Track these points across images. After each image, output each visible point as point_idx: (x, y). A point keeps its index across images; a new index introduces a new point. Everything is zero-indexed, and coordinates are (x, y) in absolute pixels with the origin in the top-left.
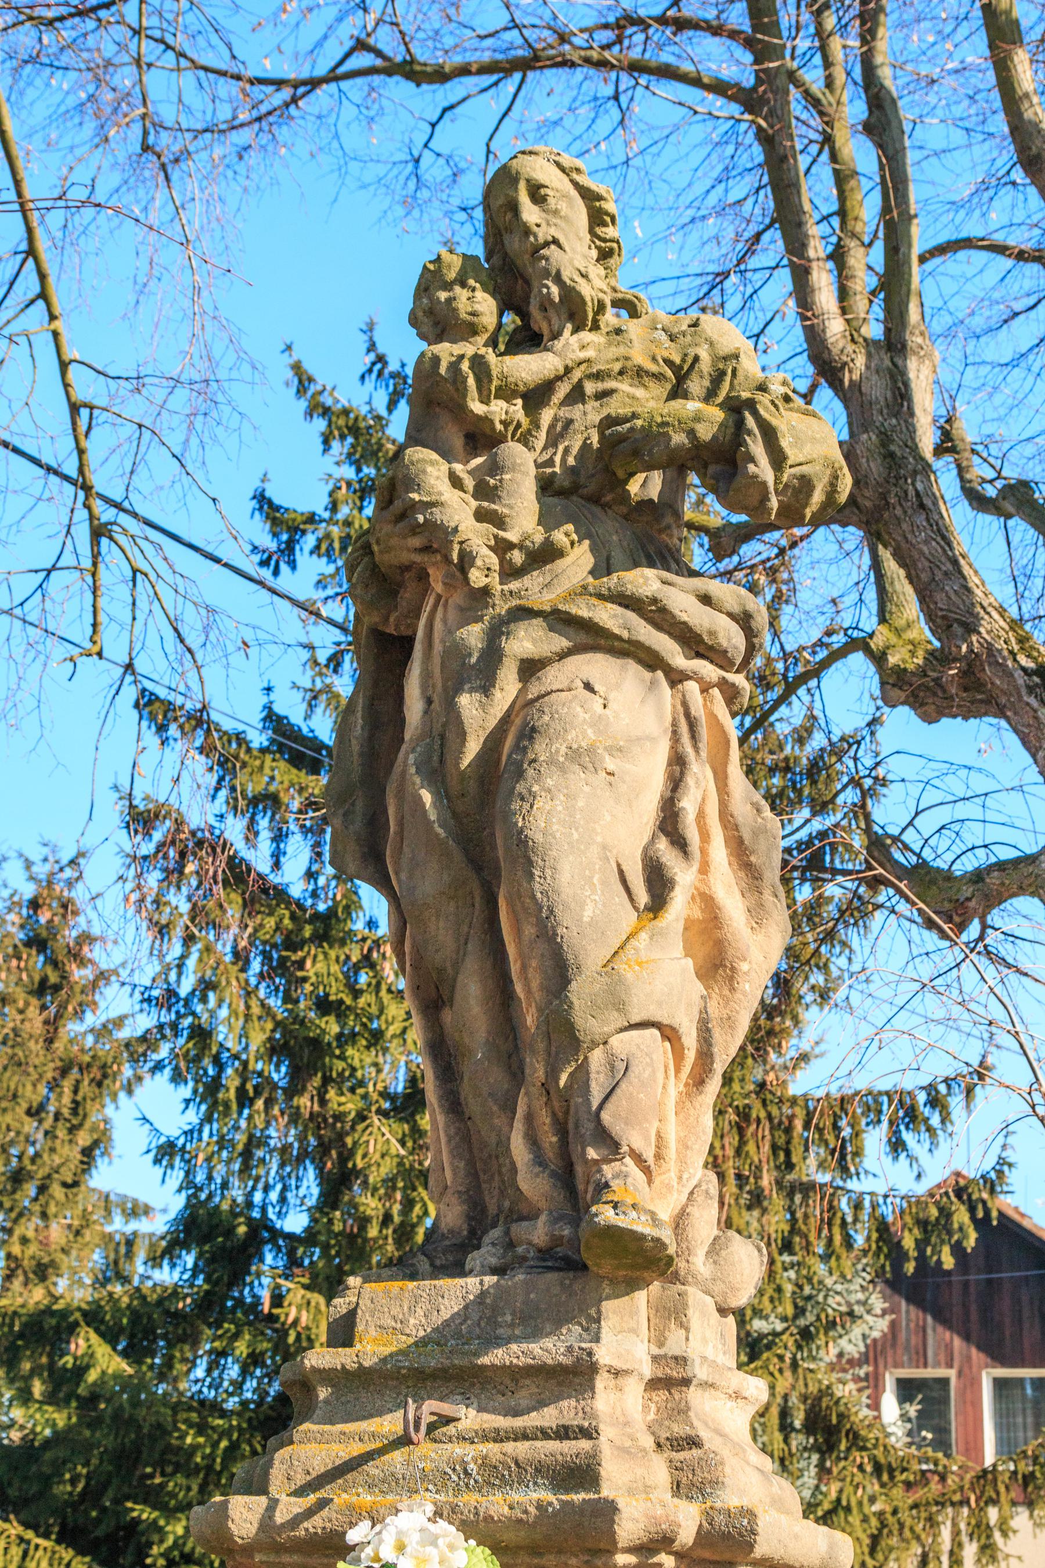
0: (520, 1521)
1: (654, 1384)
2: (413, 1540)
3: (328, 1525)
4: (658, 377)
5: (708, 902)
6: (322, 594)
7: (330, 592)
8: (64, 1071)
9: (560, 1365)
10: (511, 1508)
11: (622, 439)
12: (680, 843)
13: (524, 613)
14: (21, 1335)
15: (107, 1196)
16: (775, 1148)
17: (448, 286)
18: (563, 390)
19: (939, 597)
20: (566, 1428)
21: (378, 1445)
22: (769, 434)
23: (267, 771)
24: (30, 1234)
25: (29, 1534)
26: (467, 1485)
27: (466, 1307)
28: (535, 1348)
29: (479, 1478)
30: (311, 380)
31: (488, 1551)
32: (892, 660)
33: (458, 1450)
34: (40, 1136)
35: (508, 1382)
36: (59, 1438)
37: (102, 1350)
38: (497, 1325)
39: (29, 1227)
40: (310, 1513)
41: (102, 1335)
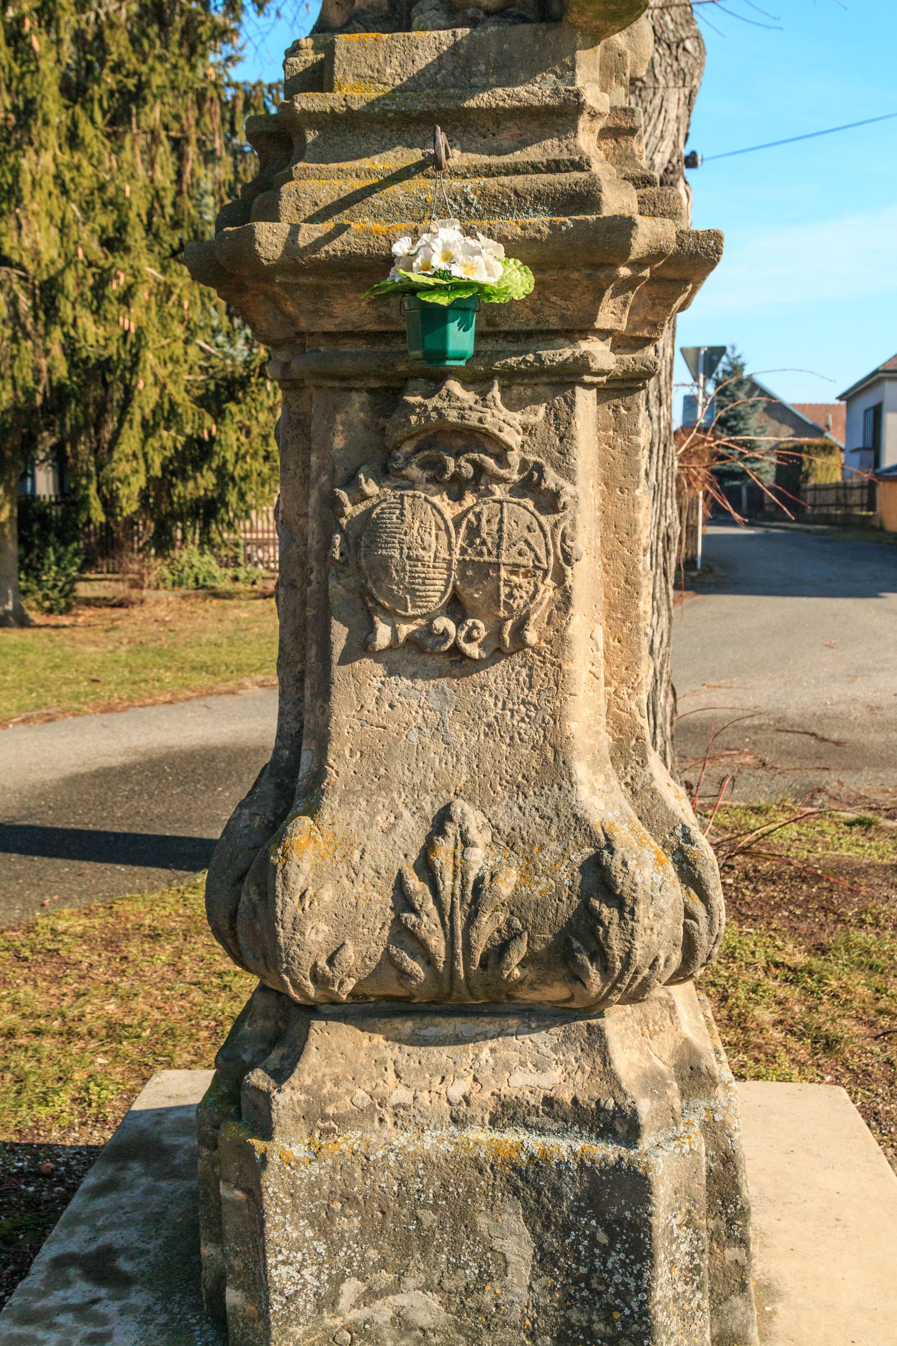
0: (534, 240)
2: (456, 252)
3: (347, 248)
9: (547, 106)
10: (523, 228)
16: (223, 119)
20: (557, 162)
21: (375, 181)
26: (468, 213)
27: (440, 58)
28: (521, 90)
29: (480, 207)
31: (519, 263)
35: (490, 125)
38: (472, 75)
40: (330, 237)
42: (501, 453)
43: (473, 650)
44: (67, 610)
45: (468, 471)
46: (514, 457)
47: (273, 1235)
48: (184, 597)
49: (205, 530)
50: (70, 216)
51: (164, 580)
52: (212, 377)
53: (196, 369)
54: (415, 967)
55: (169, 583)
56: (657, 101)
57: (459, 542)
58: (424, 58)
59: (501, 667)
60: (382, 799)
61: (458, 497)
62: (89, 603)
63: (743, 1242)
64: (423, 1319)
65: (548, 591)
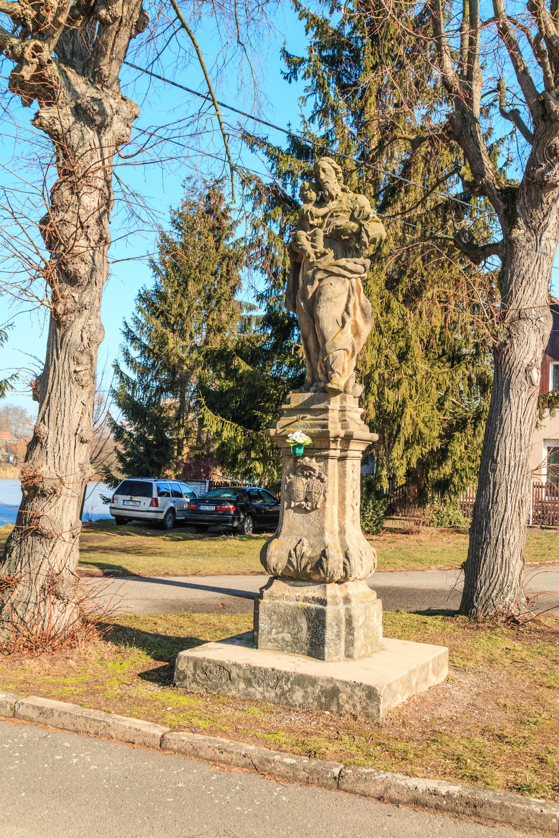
1: (340, 411)
2: (298, 436)
4: (349, 212)
5: (355, 322)
6: (306, 94)
7: (309, 93)
8: (223, 259)
11: (338, 230)
12: (348, 313)
13: (319, 269)
14: (216, 357)
15: (241, 303)
17: (306, 191)
18: (329, 214)
19: (474, 166)
22: (366, 232)
23: (289, 161)
24: (215, 317)
25: (224, 419)
30: (300, 5)
32: (465, 178)
33: (307, 422)
34: (216, 283)
36: (230, 390)
37: (243, 364)
39: (214, 315)
41: (242, 358)
42: (314, 471)
43: (308, 508)
44: (377, 532)
45: (308, 474)
46: (317, 472)
47: (260, 617)
48: (441, 531)
49: (442, 495)
50: (383, 344)
51: (433, 522)
52: (456, 418)
53: (448, 413)
54: (291, 568)
55: (435, 524)
56: (525, 340)
57: (306, 487)
58: (306, 398)
59: (314, 512)
60: (290, 537)
61: (307, 479)
62: (391, 530)
63: (353, 635)
64: (287, 639)
65: (322, 498)
